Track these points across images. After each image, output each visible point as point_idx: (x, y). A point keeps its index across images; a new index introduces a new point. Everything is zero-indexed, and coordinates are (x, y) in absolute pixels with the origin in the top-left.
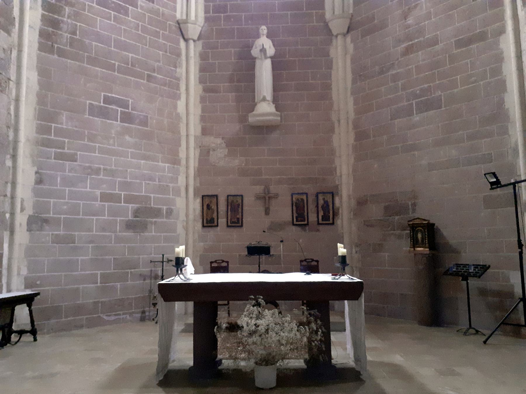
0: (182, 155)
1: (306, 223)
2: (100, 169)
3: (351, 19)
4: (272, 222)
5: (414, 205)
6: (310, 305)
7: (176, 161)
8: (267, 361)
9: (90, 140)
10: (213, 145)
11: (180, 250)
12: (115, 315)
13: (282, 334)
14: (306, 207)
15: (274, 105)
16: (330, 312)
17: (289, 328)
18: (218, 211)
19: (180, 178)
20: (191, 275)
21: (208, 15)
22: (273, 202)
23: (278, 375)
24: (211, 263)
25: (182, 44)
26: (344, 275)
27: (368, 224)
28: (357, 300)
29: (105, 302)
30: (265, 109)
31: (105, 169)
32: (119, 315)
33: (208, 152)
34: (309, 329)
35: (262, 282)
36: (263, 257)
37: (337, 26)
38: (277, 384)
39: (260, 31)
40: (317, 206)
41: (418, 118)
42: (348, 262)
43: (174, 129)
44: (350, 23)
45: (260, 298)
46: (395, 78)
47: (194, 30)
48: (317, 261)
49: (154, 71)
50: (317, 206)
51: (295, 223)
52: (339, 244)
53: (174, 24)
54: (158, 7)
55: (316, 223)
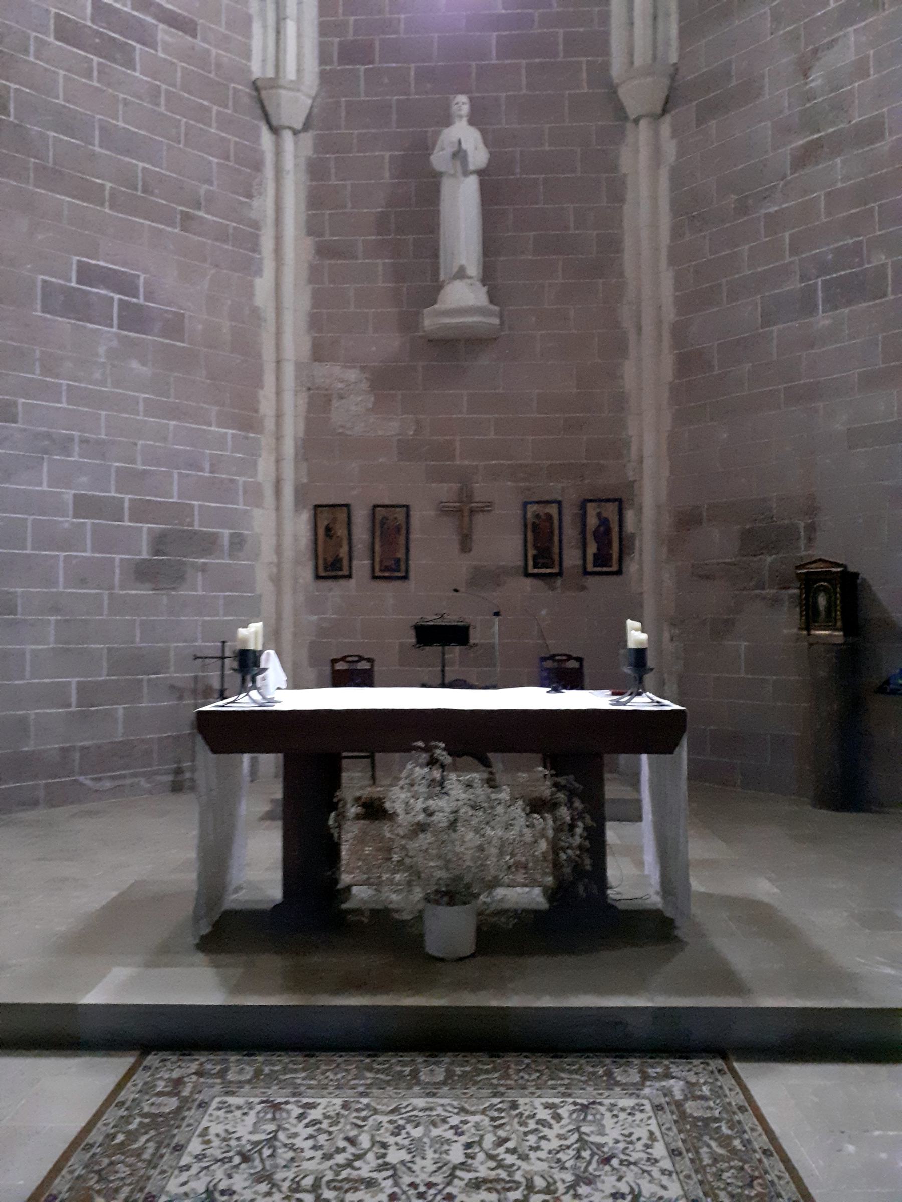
0: (267, 407)
1: (555, 570)
2: (71, 439)
3: (673, 77)
4: (476, 568)
5: (812, 528)
6: (557, 762)
7: (246, 421)
8: (452, 894)
9: (47, 370)
10: (340, 385)
11: (251, 633)
12: (113, 778)
13: (489, 832)
14: (556, 532)
15: (485, 289)
16: (607, 776)
17: (505, 819)
18: (352, 543)
20: (279, 691)
21: (328, 67)
22: (479, 518)
23: (479, 930)
24: (334, 661)
26: (639, 694)
27: (703, 575)
28: (671, 752)
29: (88, 748)
30: (463, 297)
31: (84, 441)
32: (123, 777)
33: (328, 399)
34: (554, 822)
35: (446, 709)
36: (455, 652)
37: (638, 95)
38: (477, 944)
39: (454, 108)
40: (583, 532)
41: (827, 322)
42: (651, 662)
43: (245, 345)
44: (672, 89)
45: (437, 747)
46: (774, 223)
47: (294, 106)
48: (580, 660)
49: (198, 206)
50: (583, 532)
51: (531, 570)
52: (629, 622)
53: (247, 90)
54: (207, 46)
55: (581, 570)
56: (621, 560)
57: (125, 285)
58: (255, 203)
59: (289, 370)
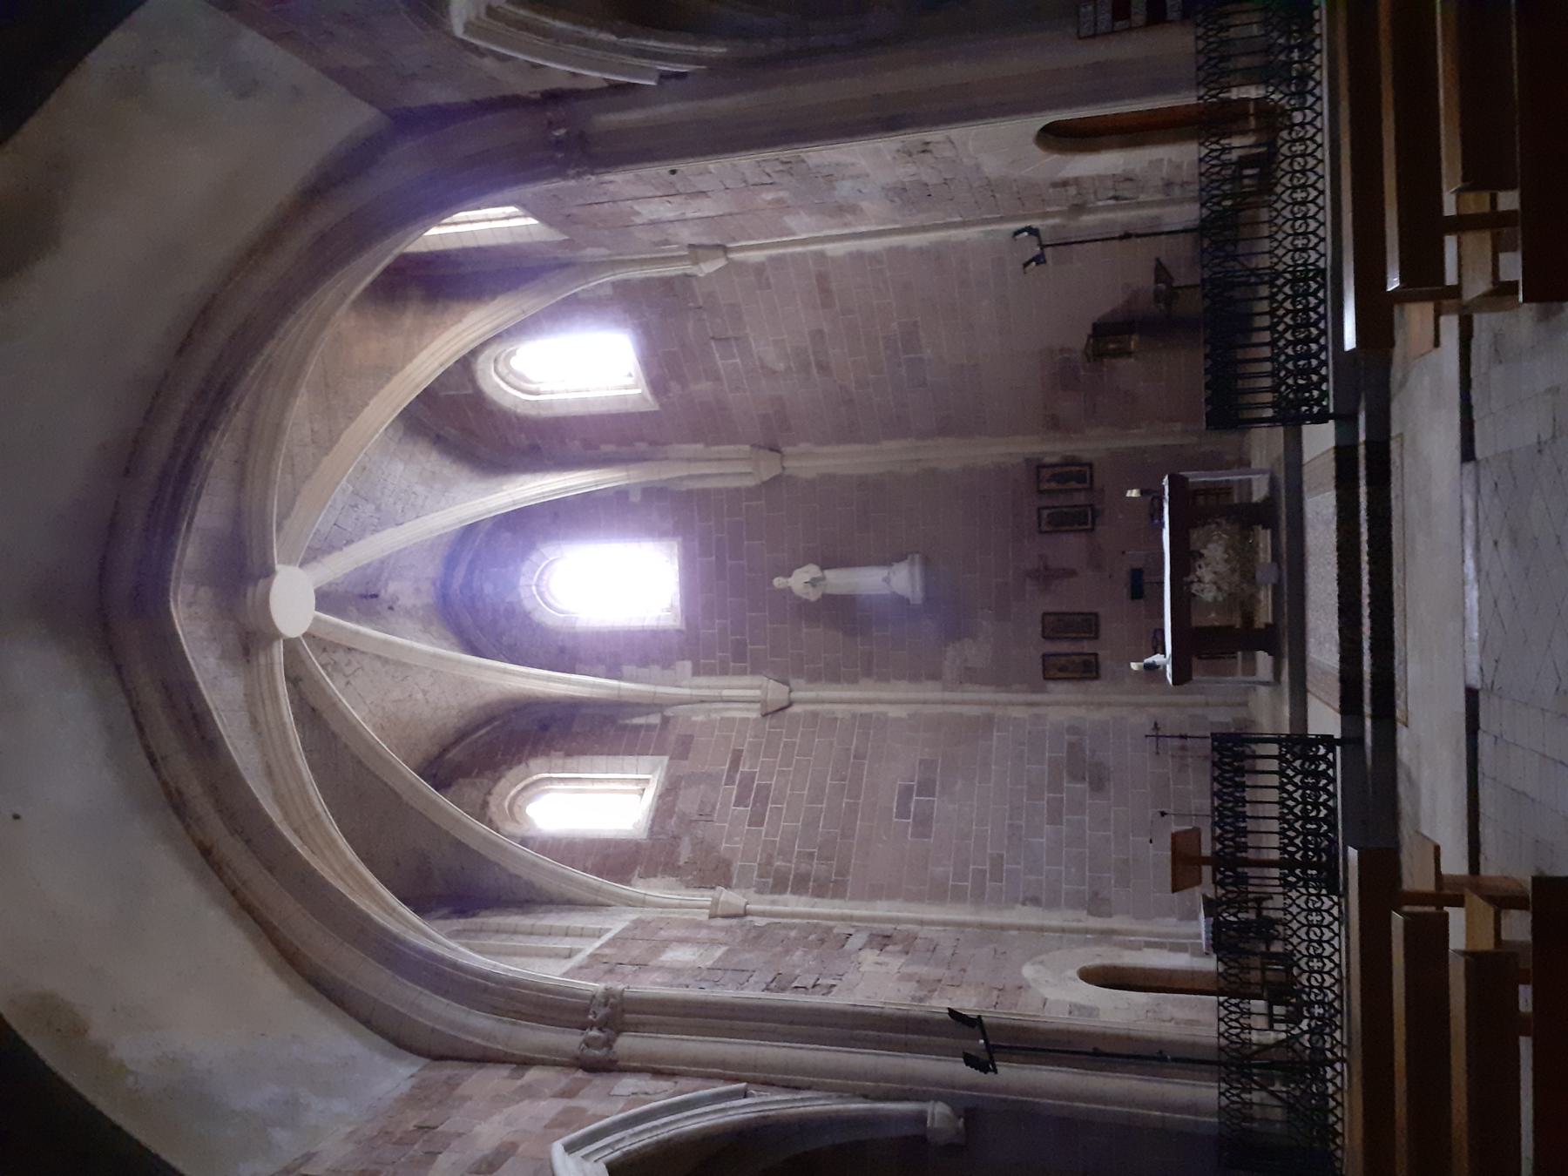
0: (975, 711)
3: (760, 447)
7: (990, 719)
19: (1014, 714)
25: (796, 709)
33: (967, 669)
36: (1146, 578)
37: (768, 468)
47: (775, 691)
50: (1060, 491)
56: (1081, 465)
57: (906, 793)
58: (840, 716)
59: (948, 695)
